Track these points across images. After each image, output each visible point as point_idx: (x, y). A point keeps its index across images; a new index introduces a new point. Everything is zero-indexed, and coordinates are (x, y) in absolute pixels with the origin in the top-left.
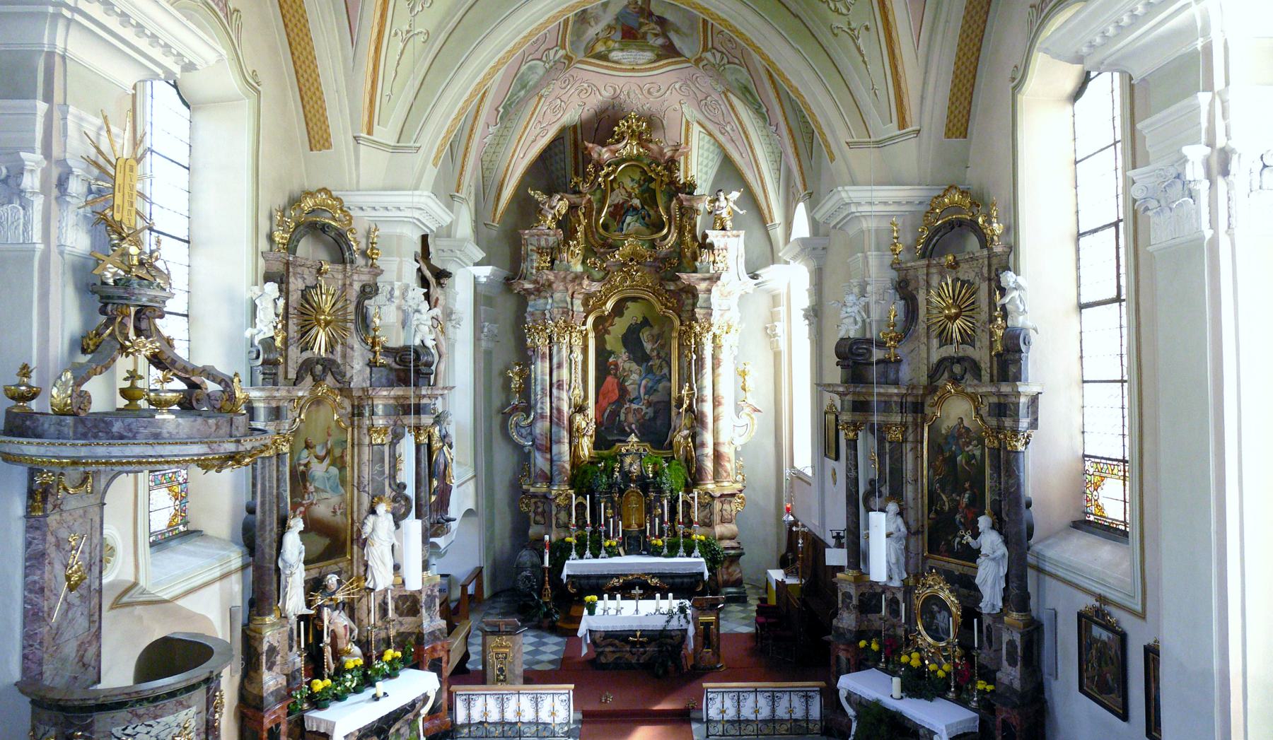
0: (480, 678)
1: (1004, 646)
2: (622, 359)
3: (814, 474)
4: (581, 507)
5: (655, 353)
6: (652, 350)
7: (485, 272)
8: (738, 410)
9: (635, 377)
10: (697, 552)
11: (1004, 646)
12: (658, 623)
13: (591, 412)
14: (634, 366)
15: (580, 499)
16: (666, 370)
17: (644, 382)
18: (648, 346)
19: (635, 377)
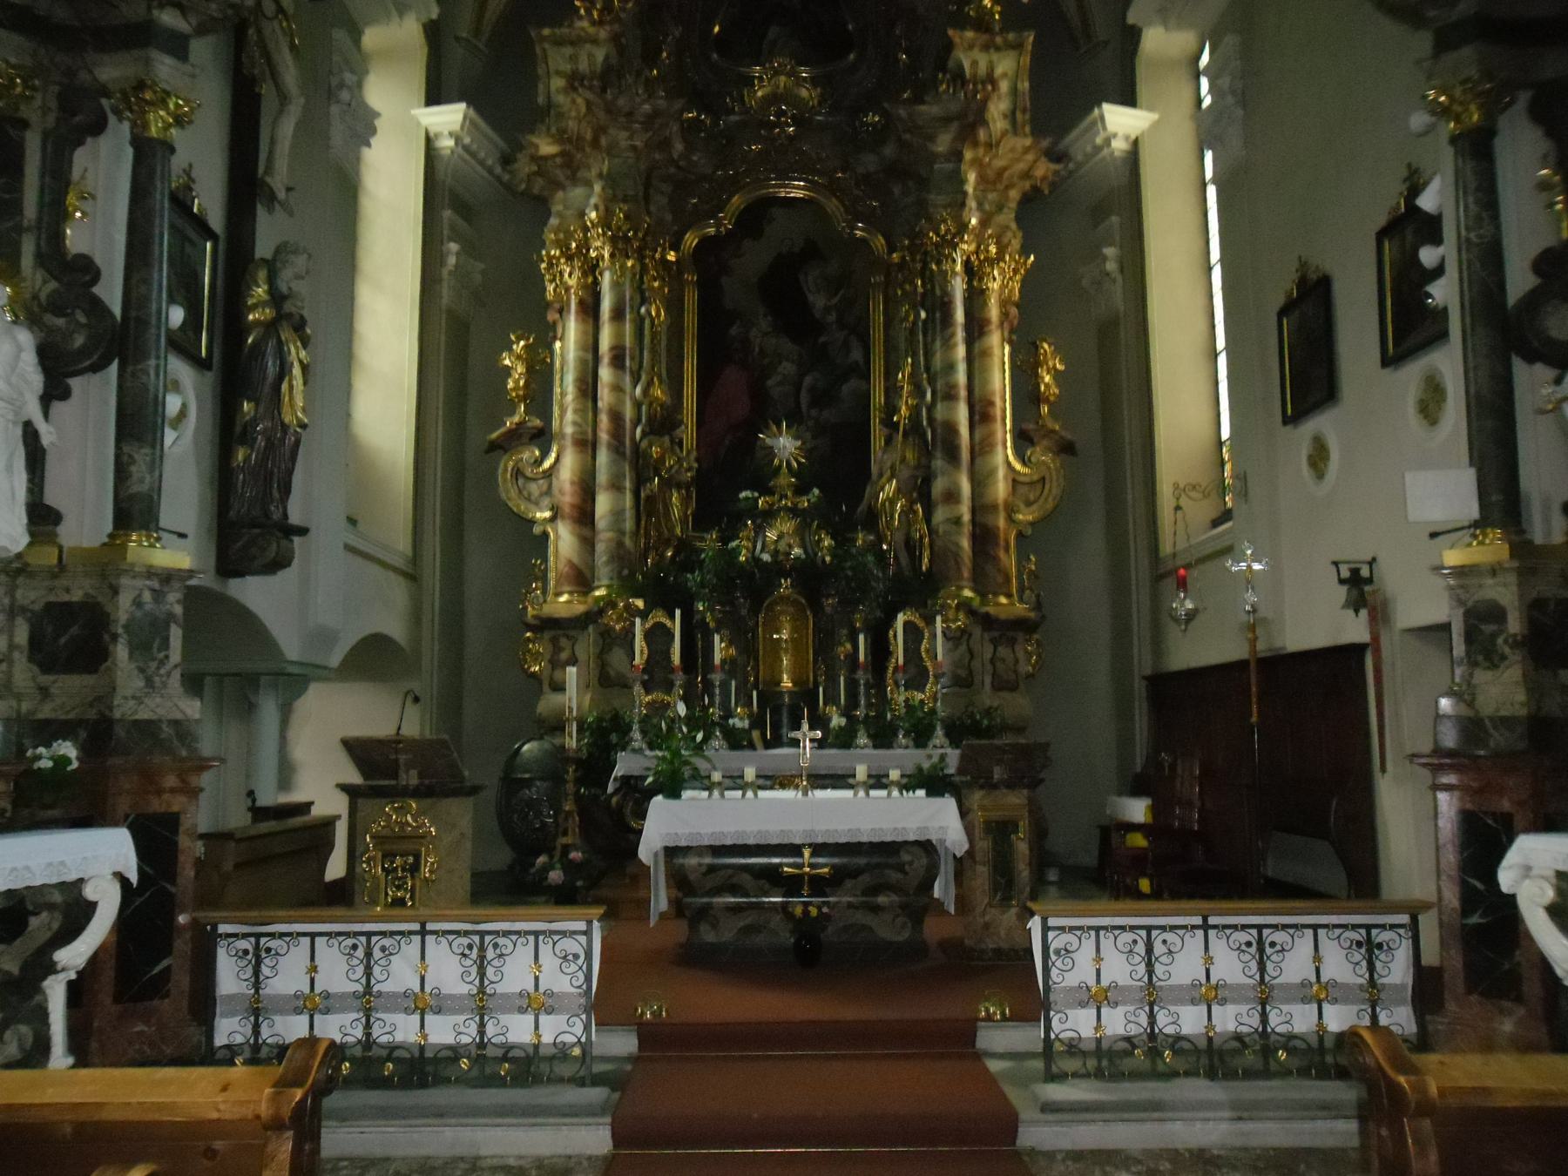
0: (1474, 699)
1: (705, 900)
2: (761, 332)
3: (1514, 306)
4: (657, 636)
5: (832, 318)
6: (827, 310)
7: (448, 119)
8: (1023, 439)
9: (787, 368)
10: (939, 736)
11: (705, 900)
12: (1330, 1142)
13: (688, 432)
14: (787, 346)
15: (659, 617)
16: (856, 355)
17: (808, 380)
18: (818, 301)
19: (787, 368)
